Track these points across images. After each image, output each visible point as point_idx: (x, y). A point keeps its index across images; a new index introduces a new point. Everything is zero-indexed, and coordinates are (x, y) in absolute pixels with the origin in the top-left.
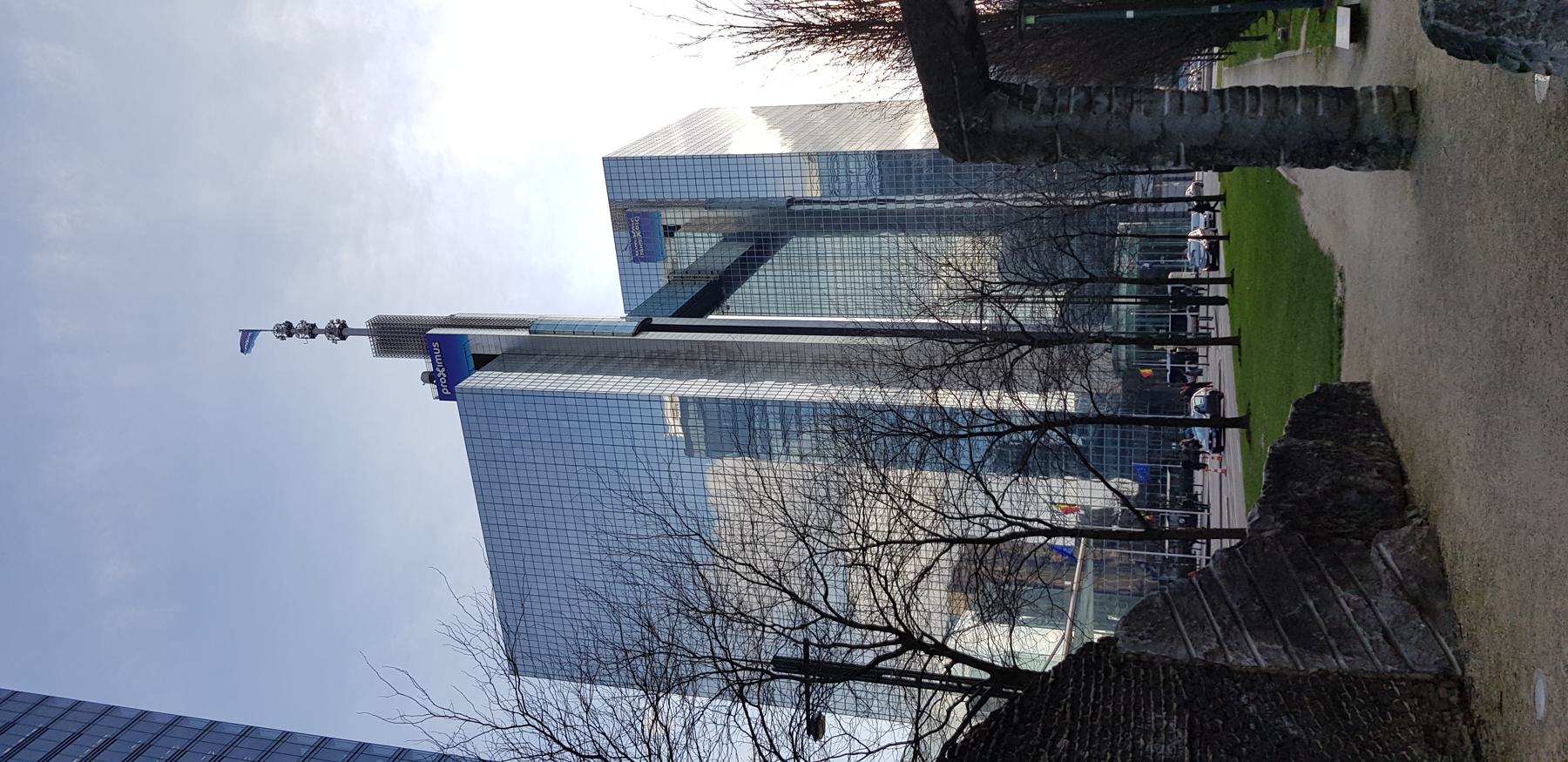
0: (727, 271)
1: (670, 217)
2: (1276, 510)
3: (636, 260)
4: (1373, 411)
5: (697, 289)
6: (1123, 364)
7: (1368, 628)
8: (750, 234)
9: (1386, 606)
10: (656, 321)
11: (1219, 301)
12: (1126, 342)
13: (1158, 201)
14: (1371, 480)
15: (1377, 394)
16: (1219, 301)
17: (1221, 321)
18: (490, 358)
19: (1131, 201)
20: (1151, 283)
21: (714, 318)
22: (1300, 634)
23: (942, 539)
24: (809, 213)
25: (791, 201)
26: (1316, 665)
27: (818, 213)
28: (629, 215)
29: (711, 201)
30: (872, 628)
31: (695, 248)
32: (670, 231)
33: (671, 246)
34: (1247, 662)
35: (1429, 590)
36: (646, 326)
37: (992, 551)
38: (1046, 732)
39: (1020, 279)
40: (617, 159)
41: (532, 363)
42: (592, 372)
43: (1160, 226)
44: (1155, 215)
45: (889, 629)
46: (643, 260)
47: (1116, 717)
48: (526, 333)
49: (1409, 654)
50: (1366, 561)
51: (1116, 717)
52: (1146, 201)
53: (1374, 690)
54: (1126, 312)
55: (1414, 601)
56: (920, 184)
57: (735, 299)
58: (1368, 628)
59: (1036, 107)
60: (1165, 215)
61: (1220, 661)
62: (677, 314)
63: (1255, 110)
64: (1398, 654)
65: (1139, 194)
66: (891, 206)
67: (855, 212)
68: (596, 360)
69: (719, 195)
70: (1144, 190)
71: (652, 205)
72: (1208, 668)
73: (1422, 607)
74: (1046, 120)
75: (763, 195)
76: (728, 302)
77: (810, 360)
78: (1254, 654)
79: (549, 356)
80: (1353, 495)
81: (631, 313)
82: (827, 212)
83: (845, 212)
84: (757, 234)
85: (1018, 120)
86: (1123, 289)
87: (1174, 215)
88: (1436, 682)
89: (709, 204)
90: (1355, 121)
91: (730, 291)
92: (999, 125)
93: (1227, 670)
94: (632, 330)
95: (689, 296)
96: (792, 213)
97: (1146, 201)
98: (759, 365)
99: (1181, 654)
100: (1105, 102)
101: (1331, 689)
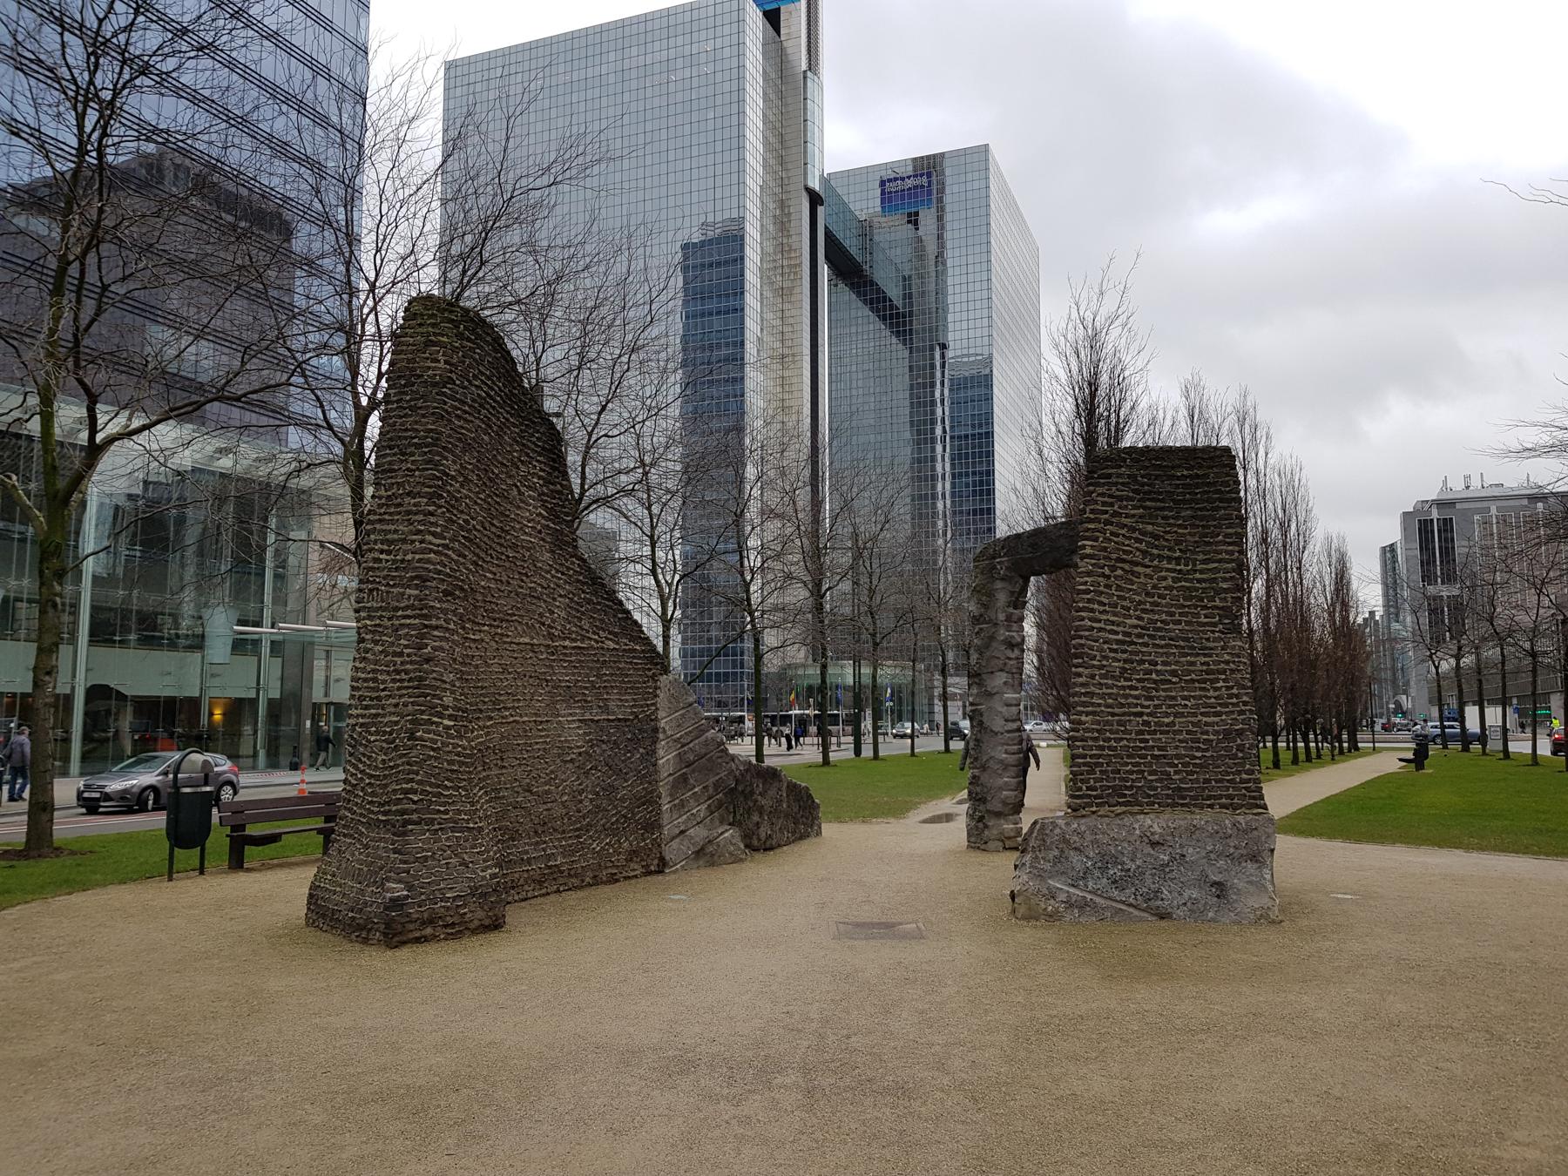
0: (872, 283)
1: (927, 218)
2: (747, 771)
3: (883, 183)
4: (803, 837)
5: (853, 251)
6: (790, 672)
7: (685, 822)
8: (911, 304)
9: (699, 833)
10: (820, 209)
11: (858, 752)
12: (823, 674)
13: (945, 697)
14: (764, 831)
15: (812, 840)
16: (858, 752)
17: (842, 750)
18: (777, 30)
19: (944, 673)
20: (865, 698)
21: (824, 271)
22: (681, 782)
23: (653, 528)
24: (933, 366)
25: (944, 347)
26: (664, 790)
27: (933, 376)
28: (929, 175)
29: (944, 264)
30: (583, 477)
31: (893, 234)
32: (913, 220)
33: (898, 219)
34: (661, 752)
35: (706, 855)
36: (815, 199)
37: (645, 571)
38: (616, 635)
39: (875, 582)
40: (987, 160)
41: (773, 76)
42: (766, 142)
43: (921, 700)
44: (931, 698)
45: (583, 491)
46: (883, 193)
47: (627, 675)
48: (804, 67)
49: (674, 844)
50: (721, 823)
51: (627, 675)
52: (944, 688)
53: (653, 826)
54: (844, 673)
55: (702, 849)
56: (959, 437)
57: (846, 294)
58: (685, 822)
59: (1011, 610)
60: (931, 705)
61: (661, 736)
62: (828, 234)
63: (1006, 752)
64: (673, 839)
65: (950, 680)
66: (939, 448)
67: (933, 413)
68: (778, 146)
69: (950, 271)
70: (953, 685)
71: (940, 200)
72: (656, 730)
73: (699, 853)
74: (1002, 617)
75: (950, 318)
76: (841, 285)
77: (786, 373)
78: (666, 757)
79: (781, 96)
80: (756, 818)
81: (826, 181)
82: (933, 385)
83: (933, 403)
84: (911, 313)
85: (1002, 598)
86: (866, 670)
87: (932, 713)
88: (662, 859)
89: (940, 257)
90: (998, 815)
91: (852, 286)
92: (999, 585)
93: (655, 741)
94: (810, 184)
95: (847, 244)
96: (932, 349)
97: (944, 688)
98: (779, 322)
99: (661, 714)
100: (1013, 656)
101: (649, 800)
